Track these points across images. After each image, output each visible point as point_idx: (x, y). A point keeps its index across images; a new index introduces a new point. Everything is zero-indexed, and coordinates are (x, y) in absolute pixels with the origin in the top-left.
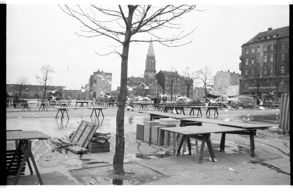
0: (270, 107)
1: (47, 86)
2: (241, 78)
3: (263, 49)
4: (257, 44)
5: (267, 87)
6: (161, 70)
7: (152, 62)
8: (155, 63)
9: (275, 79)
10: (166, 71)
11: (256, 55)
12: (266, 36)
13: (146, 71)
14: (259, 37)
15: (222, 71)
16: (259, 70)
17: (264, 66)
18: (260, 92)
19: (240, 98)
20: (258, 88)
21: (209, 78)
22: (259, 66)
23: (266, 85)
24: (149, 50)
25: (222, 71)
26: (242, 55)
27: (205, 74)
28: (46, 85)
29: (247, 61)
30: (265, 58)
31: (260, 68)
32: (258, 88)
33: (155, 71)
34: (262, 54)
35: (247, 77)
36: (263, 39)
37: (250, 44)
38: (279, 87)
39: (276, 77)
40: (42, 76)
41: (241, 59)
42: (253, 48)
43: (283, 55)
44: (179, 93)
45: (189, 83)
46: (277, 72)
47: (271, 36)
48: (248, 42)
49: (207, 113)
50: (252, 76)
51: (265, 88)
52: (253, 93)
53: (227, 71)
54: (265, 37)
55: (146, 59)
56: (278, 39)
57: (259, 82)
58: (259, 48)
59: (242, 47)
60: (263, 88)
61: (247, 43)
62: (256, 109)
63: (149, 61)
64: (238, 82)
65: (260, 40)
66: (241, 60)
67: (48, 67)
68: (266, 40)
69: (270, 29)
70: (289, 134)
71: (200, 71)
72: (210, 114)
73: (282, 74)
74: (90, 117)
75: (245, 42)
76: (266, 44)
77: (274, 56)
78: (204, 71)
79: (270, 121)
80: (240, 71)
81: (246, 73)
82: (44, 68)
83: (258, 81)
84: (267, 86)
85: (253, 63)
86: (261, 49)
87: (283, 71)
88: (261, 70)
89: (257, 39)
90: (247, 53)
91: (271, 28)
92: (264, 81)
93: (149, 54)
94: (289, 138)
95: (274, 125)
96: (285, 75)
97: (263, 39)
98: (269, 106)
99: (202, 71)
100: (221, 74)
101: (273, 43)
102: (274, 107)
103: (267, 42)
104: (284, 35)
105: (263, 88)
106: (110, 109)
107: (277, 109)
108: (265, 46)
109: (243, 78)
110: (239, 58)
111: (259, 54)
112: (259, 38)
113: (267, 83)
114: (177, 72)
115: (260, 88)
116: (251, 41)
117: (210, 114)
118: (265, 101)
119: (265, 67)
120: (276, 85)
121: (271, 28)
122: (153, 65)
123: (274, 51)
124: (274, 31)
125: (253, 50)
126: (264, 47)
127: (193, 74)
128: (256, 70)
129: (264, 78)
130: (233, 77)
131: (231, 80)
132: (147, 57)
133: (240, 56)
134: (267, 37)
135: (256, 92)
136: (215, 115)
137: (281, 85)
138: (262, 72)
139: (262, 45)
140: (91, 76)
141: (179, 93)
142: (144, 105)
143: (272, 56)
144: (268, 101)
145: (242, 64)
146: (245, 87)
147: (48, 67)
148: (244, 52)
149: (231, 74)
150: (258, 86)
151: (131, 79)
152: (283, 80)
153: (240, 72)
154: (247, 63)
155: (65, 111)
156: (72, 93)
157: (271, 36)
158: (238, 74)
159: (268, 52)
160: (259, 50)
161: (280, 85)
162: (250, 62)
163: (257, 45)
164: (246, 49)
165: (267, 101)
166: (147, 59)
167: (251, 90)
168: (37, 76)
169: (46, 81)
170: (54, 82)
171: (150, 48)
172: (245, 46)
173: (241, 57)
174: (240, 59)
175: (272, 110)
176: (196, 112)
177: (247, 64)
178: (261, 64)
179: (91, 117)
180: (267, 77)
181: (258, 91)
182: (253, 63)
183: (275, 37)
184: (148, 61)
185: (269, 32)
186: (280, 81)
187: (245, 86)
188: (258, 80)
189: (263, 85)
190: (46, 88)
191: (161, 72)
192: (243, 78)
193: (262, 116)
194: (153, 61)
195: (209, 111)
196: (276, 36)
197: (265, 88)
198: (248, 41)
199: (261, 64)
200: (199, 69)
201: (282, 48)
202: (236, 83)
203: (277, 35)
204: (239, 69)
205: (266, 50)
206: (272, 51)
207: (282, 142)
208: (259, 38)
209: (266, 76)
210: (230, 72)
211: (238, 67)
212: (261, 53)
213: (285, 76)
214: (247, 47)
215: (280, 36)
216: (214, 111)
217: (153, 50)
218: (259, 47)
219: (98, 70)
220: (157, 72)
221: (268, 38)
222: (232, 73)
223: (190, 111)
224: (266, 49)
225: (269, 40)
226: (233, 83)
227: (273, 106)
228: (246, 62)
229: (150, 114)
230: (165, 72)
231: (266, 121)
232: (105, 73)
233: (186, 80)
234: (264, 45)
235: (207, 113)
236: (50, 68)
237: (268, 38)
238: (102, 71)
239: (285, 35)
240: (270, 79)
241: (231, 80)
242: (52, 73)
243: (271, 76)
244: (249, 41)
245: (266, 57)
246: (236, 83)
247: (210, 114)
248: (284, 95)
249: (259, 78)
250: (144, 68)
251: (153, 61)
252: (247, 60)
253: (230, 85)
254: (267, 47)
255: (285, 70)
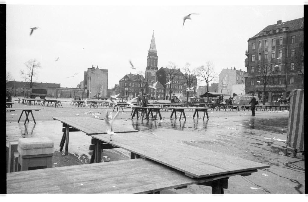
0: (277, 108)
1: (33, 83)
2: (247, 76)
3: (271, 44)
4: (264, 38)
5: (275, 86)
6: (162, 67)
7: (153, 59)
8: (157, 59)
9: (285, 76)
10: (169, 68)
11: (265, 49)
12: (275, 29)
13: (148, 68)
14: (268, 30)
15: (228, 69)
16: (266, 67)
17: (272, 61)
18: (267, 92)
19: (242, 97)
20: (265, 87)
21: (211, 75)
22: (266, 62)
23: (274, 83)
24: (150, 46)
25: (228, 68)
26: (248, 50)
27: (207, 71)
28: (32, 82)
29: (253, 57)
30: (273, 53)
31: (268, 65)
32: (265, 87)
33: (157, 68)
34: (270, 49)
35: (253, 74)
36: (271, 32)
37: (257, 38)
38: (288, 85)
39: (285, 74)
40: (27, 71)
41: (248, 54)
42: (260, 42)
43: (294, 50)
44: (181, 91)
45: (191, 80)
46: (287, 69)
47: (280, 30)
48: (255, 36)
49: (194, 116)
50: (259, 73)
51: (272, 86)
52: (260, 93)
53: (233, 69)
54: (274, 31)
55: (147, 55)
56: (288, 33)
57: (266, 80)
58: (267, 42)
59: (248, 41)
60: (270, 86)
61: (253, 37)
62: (260, 111)
63: (151, 57)
64: (244, 80)
65: (268, 34)
66: (247, 56)
67: (35, 61)
68: (274, 33)
69: (279, 22)
70: (304, 156)
71: (202, 68)
72: (198, 118)
73: (292, 71)
74: (17, 122)
75: (252, 36)
76: (275, 38)
77: (283, 52)
78: (206, 67)
79: (276, 128)
80: (246, 68)
81: (252, 70)
82: (30, 63)
83: (265, 78)
84: (276, 84)
85: (260, 59)
86: (269, 43)
87: (293, 68)
88: (268, 67)
89: (265, 33)
90: (254, 48)
91: (281, 21)
92: (272, 79)
93: (151, 50)
94: (302, 165)
95: (281, 135)
96: (294, 72)
97: (271, 32)
98: (276, 107)
99: (204, 67)
100: (226, 71)
101: (282, 37)
102: (282, 108)
103: (276, 35)
104: (294, 28)
105: (270, 86)
106: (78, 109)
107: (286, 111)
108: (273, 40)
109: (249, 76)
110: (245, 53)
111: (267, 49)
112: (267, 31)
113: (275, 81)
114: (179, 69)
115: (267, 86)
116: (259, 35)
117: (198, 118)
118: (273, 101)
119: (273, 63)
120: (285, 84)
121: (281, 21)
122: (155, 62)
123: (283, 46)
124: (284, 23)
125: (261, 44)
126: (273, 41)
127: (194, 70)
128: (263, 67)
129: (272, 75)
130: (239, 75)
131: (238, 78)
132: (148, 53)
133: (246, 51)
134: (275, 31)
135: (263, 91)
136: (203, 119)
137: (291, 83)
138: (270, 68)
139: (270, 39)
140: (85, 72)
141: (181, 91)
142: (94, 103)
143: (281, 51)
144: (276, 101)
145: (248, 60)
146: (251, 85)
147: (35, 61)
148: (250, 46)
149: (237, 72)
150: (265, 84)
151: (129, 76)
152: (293, 78)
153: (245, 69)
154: (253, 59)
155: (30, 113)
156: (62, 91)
157: (280, 30)
158: (245, 72)
159: (277, 47)
160: (267, 45)
161: (290, 84)
162: (257, 58)
163: (266, 39)
164: (252, 43)
165: (274, 101)
166: (149, 56)
167: (257, 88)
168: (21, 72)
169: (32, 77)
170: (41, 78)
171: (152, 44)
172: (252, 41)
173: (247, 52)
174: (246, 55)
175: (280, 111)
176: (178, 114)
177: (254, 61)
178: (269, 60)
179: (18, 122)
180: (274, 75)
181: (264, 90)
182: (260, 59)
183: (284, 30)
184: (149, 58)
185: (278, 25)
186: (290, 79)
187: (252, 85)
188: (265, 77)
189: (271, 84)
190: (31, 84)
191: (162, 68)
192: (249, 76)
193: (266, 120)
194: (155, 58)
195: (174, 113)
196: (286, 30)
197: (272, 86)
198: (255, 35)
199: (269, 60)
200: (201, 65)
201: (292, 43)
202: (242, 81)
203: (287, 28)
204: (244, 65)
205: (275, 45)
206: (281, 45)
207: (291, 180)
208: (267, 32)
209: (273, 74)
210: (236, 69)
211: (244, 64)
212: (269, 48)
213: (294, 73)
214: (253, 41)
215: (290, 29)
216: (180, 113)
217: (155, 46)
218: (266, 41)
219: (93, 67)
220: (159, 69)
221: (277, 31)
222: (239, 71)
223: (171, 113)
224: (274, 44)
225: (278, 33)
226: (239, 82)
227: (280, 107)
228: (252, 57)
229: (62, 122)
230: (167, 69)
231: (271, 127)
232: (100, 69)
233: (170, 72)
234: (273, 39)
235: (194, 116)
236: (36, 63)
237: (277, 31)
238: (97, 67)
239: (295, 28)
240: (279, 77)
241: (238, 78)
242: (38, 68)
243: (280, 74)
244: (257, 35)
245: (274, 52)
246: (242, 81)
247: (199, 117)
248: (296, 91)
249: (266, 76)
250: (145, 65)
251: (155, 58)
252: (254, 55)
253: (236, 83)
254: (275, 42)
255: (295, 67)
